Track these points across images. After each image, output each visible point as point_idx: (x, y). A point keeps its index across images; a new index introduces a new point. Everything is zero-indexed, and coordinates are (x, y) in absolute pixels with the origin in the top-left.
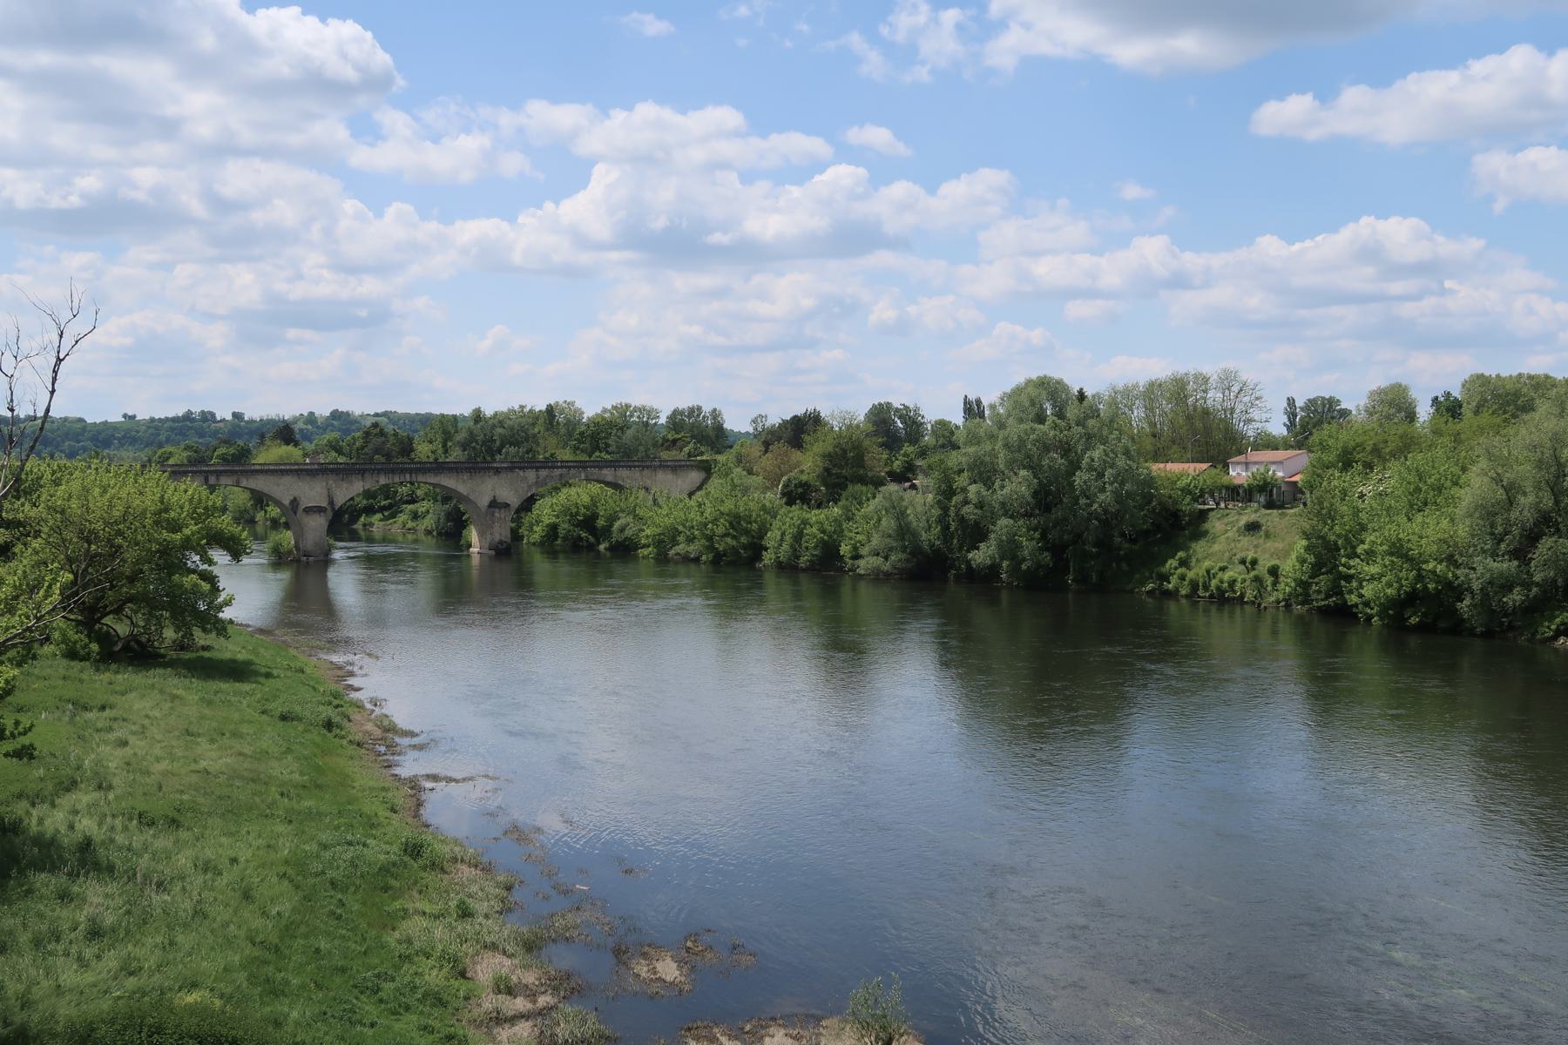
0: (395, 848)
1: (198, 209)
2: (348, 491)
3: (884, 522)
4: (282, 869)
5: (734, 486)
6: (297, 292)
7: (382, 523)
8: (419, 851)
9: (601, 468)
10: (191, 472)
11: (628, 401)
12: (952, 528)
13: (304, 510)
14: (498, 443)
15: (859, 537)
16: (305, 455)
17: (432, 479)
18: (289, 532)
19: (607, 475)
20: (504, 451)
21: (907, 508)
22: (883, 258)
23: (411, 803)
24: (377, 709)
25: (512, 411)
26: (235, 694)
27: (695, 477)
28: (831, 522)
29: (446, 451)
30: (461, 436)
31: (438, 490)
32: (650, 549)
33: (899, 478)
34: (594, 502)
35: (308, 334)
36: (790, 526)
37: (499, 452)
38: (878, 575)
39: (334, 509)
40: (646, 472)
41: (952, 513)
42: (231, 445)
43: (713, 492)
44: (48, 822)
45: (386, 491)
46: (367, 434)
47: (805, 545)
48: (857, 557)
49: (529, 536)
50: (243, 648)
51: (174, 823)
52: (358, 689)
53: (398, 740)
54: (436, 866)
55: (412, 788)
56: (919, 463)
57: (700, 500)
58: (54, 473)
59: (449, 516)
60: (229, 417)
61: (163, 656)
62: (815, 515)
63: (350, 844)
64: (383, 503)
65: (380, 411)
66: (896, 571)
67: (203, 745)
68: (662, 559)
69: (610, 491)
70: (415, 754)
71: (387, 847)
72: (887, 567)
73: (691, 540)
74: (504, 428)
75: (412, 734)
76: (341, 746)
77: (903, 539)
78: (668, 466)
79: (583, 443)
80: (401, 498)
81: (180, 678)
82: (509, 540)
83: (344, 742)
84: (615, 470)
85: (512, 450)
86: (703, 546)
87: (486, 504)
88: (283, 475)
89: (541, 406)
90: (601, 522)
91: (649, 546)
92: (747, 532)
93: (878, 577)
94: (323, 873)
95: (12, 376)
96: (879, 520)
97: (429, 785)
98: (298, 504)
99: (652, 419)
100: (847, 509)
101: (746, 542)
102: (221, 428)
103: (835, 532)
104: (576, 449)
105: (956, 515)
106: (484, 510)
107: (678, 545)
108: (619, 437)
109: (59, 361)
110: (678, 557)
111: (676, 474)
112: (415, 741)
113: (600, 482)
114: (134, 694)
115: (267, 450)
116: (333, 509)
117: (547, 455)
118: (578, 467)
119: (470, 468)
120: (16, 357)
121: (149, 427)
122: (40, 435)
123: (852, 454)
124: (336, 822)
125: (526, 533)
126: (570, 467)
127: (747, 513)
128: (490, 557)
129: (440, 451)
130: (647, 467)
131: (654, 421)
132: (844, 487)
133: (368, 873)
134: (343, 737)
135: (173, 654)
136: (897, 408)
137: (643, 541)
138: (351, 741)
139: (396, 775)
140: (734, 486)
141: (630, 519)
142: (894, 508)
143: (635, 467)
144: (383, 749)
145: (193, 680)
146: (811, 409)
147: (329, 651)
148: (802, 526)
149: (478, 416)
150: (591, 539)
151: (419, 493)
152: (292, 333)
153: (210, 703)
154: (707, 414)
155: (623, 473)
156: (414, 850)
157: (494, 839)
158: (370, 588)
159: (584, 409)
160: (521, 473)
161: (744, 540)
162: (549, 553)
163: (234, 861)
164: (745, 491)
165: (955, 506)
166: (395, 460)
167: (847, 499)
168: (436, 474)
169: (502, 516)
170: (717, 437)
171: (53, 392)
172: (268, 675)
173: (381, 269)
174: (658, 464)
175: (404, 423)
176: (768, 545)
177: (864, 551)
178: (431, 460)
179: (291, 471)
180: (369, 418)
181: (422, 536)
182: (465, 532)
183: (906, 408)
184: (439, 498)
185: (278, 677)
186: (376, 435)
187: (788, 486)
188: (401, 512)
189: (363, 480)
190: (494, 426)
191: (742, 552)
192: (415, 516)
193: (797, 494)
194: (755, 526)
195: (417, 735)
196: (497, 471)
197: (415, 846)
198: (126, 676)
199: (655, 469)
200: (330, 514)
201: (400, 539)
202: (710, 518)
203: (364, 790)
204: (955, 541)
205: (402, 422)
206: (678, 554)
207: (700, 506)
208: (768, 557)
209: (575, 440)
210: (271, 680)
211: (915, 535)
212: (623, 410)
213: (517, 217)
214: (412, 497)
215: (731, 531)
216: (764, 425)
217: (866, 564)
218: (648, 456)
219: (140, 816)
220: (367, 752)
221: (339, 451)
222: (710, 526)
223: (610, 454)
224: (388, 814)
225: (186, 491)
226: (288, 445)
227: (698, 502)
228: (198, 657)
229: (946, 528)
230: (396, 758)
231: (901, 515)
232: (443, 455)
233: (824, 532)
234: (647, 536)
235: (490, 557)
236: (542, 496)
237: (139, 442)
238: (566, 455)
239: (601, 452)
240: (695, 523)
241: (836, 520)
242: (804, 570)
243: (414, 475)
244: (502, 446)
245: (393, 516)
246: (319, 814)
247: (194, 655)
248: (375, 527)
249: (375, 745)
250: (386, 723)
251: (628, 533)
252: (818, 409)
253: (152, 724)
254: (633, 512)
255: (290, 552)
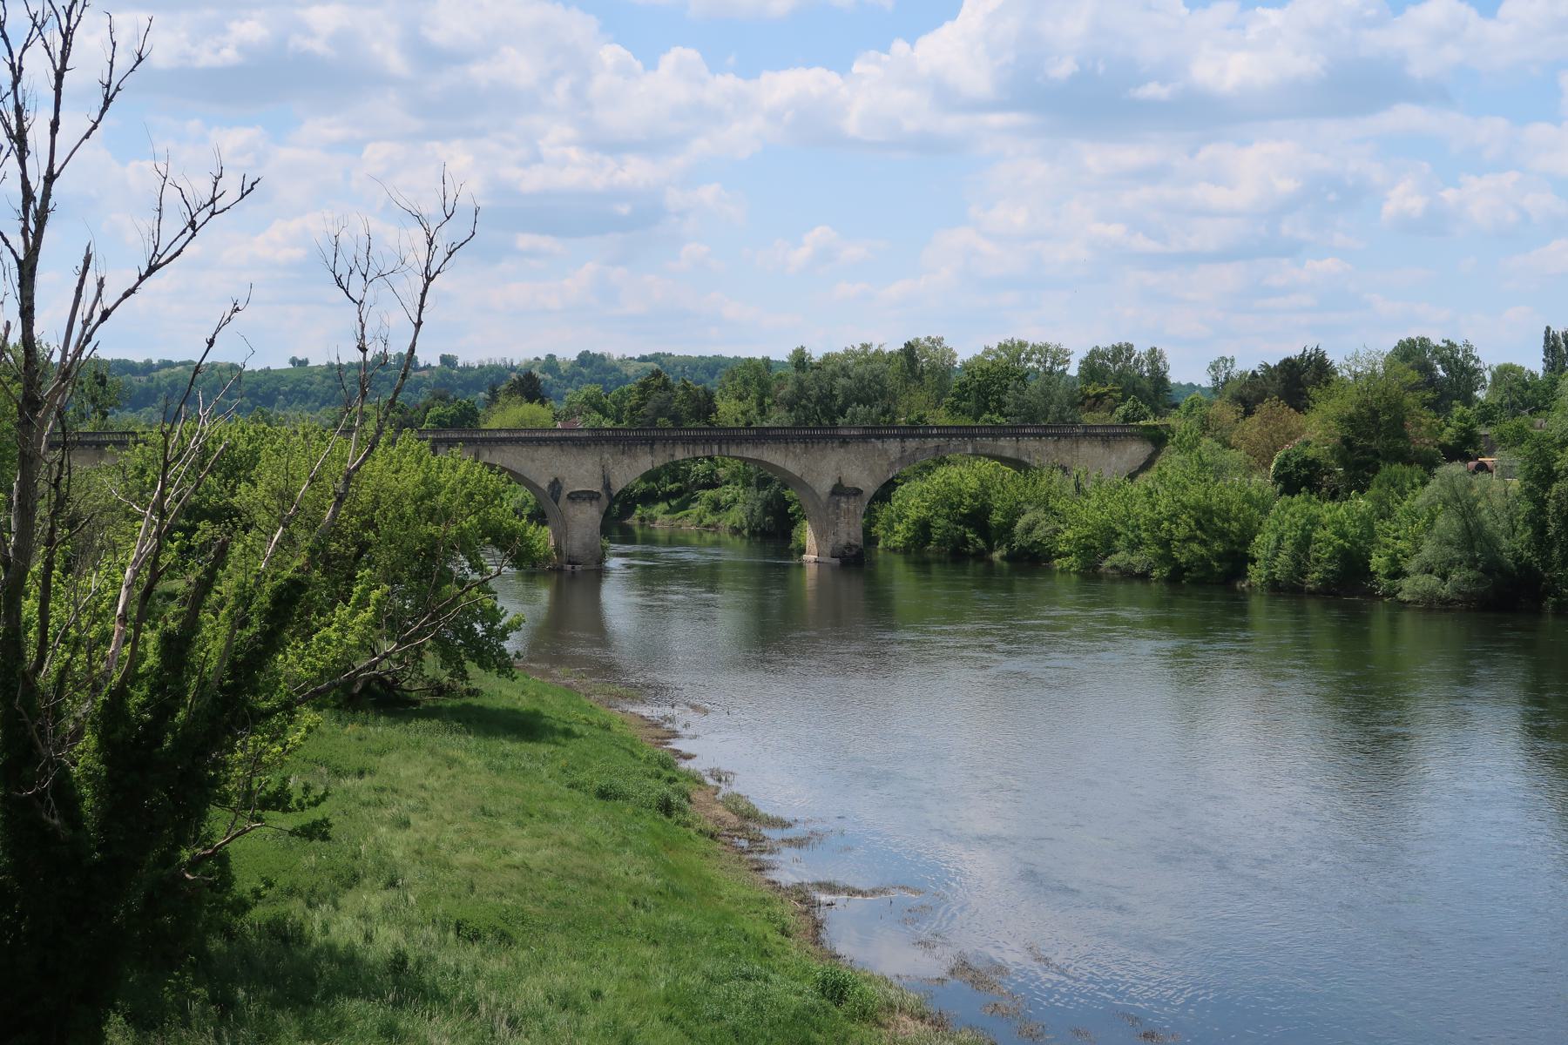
0: (807, 987)
1: (396, 62)
2: (629, 471)
3: (1441, 521)
4: (665, 1010)
5: (1203, 465)
6: (532, 180)
7: (667, 517)
8: (842, 992)
9: (996, 437)
10: (460, 440)
11: (1023, 338)
12: (1551, 532)
13: (569, 496)
14: (840, 401)
15: (1400, 545)
16: (556, 417)
17: (751, 453)
18: (546, 528)
19: (1003, 447)
20: (849, 411)
21: (1477, 500)
22: (1405, 117)
23: (806, 923)
24: (723, 785)
25: (850, 353)
26: (532, 758)
27: (1137, 451)
28: (1355, 521)
29: (762, 412)
30: (788, 390)
31: (752, 469)
32: (1072, 559)
33: (1455, 453)
34: (985, 489)
35: (545, 242)
36: (1291, 525)
37: (842, 412)
38: (1431, 602)
39: (611, 495)
40: (1063, 443)
41: (1551, 509)
42: (449, 402)
43: (1170, 473)
44: (334, 929)
45: (673, 470)
46: (645, 386)
47: (1313, 555)
48: (1397, 573)
49: (887, 538)
50: (523, 693)
51: (504, 938)
52: (688, 757)
53: (765, 832)
54: (864, 1015)
55: (801, 902)
56: (1482, 430)
57: (1150, 485)
58: (250, 440)
59: (767, 506)
60: (436, 363)
61: (416, 703)
62: (1329, 511)
63: (747, 977)
64: (669, 487)
65: (648, 352)
66: (1460, 597)
67: (510, 833)
68: (1090, 574)
69: (1010, 471)
70: (792, 852)
71: (798, 986)
72: (1446, 590)
73: (1134, 546)
74: (849, 377)
75: (783, 824)
76: (690, 837)
77: (1471, 548)
78: (1096, 435)
79: (965, 400)
80: (696, 480)
81: (451, 733)
82: (860, 543)
83: (692, 832)
84: (1018, 441)
85: (861, 410)
86: (1155, 555)
87: (828, 490)
88: (540, 445)
89: (894, 344)
90: (996, 518)
91: (1067, 555)
92: (1223, 535)
93: (1432, 606)
94: (720, 1017)
95: (361, 302)
96: (1432, 519)
97: (824, 898)
98: (561, 488)
99: (1059, 364)
100: (1380, 501)
101: (1221, 549)
102: (424, 378)
103: (1361, 536)
104: (954, 409)
105: (1558, 512)
106: (824, 498)
107: (1116, 553)
108: (1018, 391)
109: (429, 279)
110: (1115, 571)
111: (1108, 447)
112: (789, 833)
113: (992, 457)
114: (394, 756)
115: (503, 409)
116: (610, 495)
117: (913, 417)
118: (963, 436)
119: (805, 437)
120: (365, 276)
121: (327, 377)
122: (402, 384)
123: (1386, 418)
124: (717, 947)
125: (882, 533)
126: (950, 436)
127: (1223, 505)
128: (833, 568)
129: (754, 412)
130: (1066, 436)
131: (1061, 368)
132: (1376, 470)
133: (780, 1022)
134: (687, 825)
135: (429, 701)
136: (1437, 347)
137: (1062, 548)
138: (700, 831)
139: (774, 882)
140: (1203, 465)
141: (1041, 513)
142: (1458, 500)
143: (1047, 435)
144: (744, 843)
145: (470, 737)
146: (1311, 347)
147: (633, 700)
148: (1309, 527)
149: (800, 360)
150: (981, 543)
151: (722, 472)
152: (524, 241)
153: (500, 770)
154: (1143, 357)
155: (1030, 444)
156: (835, 990)
157: (938, 979)
158: (654, 612)
159: (955, 350)
160: (879, 444)
161: (1218, 546)
162: (916, 563)
163: (597, 995)
164: (1220, 471)
165: (1557, 498)
166: (686, 425)
167: (1380, 486)
168: (756, 445)
169: (851, 508)
170: (1157, 391)
171: (419, 324)
172: (568, 733)
173: (651, 145)
174: (1082, 431)
175: (683, 371)
176: (1256, 555)
177: (1411, 566)
178: (741, 424)
179: (551, 440)
180: (632, 362)
181: (725, 536)
182: (795, 532)
183: (1452, 346)
184: (753, 480)
185: (581, 736)
186: (657, 387)
187: (1285, 465)
188: (695, 500)
189: (652, 453)
190: (834, 375)
191: (1215, 564)
192: (716, 507)
193: (1299, 477)
194: (1235, 526)
195: (790, 825)
196: (845, 441)
197: (836, 985)
198: (380, 729)
199: (1077, 438)
200: (605, 502)
201: (695, 540)
202: (1165, 514)
203: (737, 903)
204: (1556, 552)
205: (679, 369)
206: (1115, 567)
207: (1150, 494)
208: (1256, 574)
209: (953, 395)
210: (574, 740)
211: (1491, 542)
212: (1015, 350)
213: (852, 65)
214: (711, 479)
215: (1198, 532)
216: (1229, 373)
217: (1412, 586)
218: (1063, 420)
219: (458, 927)
220: (725, 847)
221: (602, 411)
222: (1166, 524)
223: (1005, 416)
224: (779, 937)
225: (454, 468)
226: (532, 402)
227: (1146, 488)
228: (464, 704)
229: (1541, 529)
230: (765, 857)
231: (1468, 512)
232: (758, 418)
233: (1343, 536)
234: (1068, 541)
235: (833, 568)
236: (906, 479)
237: (313, 399)
238: (941, 418)
239: (991, 413)
240: (1141, 521)
241: (1363, 518)
242: (1311, 593)
243: (724, 447)
244: (846, 404)
245: (683, 506)
246: (692, 934)
247: (457, 702)
248: (658, 522)
249: (733, 837)
250: (742, 806)
251: (1038, 534)
252: (1322, 348)
253: (433, 799)
254: (1044, 504)
255: (547, 558)
